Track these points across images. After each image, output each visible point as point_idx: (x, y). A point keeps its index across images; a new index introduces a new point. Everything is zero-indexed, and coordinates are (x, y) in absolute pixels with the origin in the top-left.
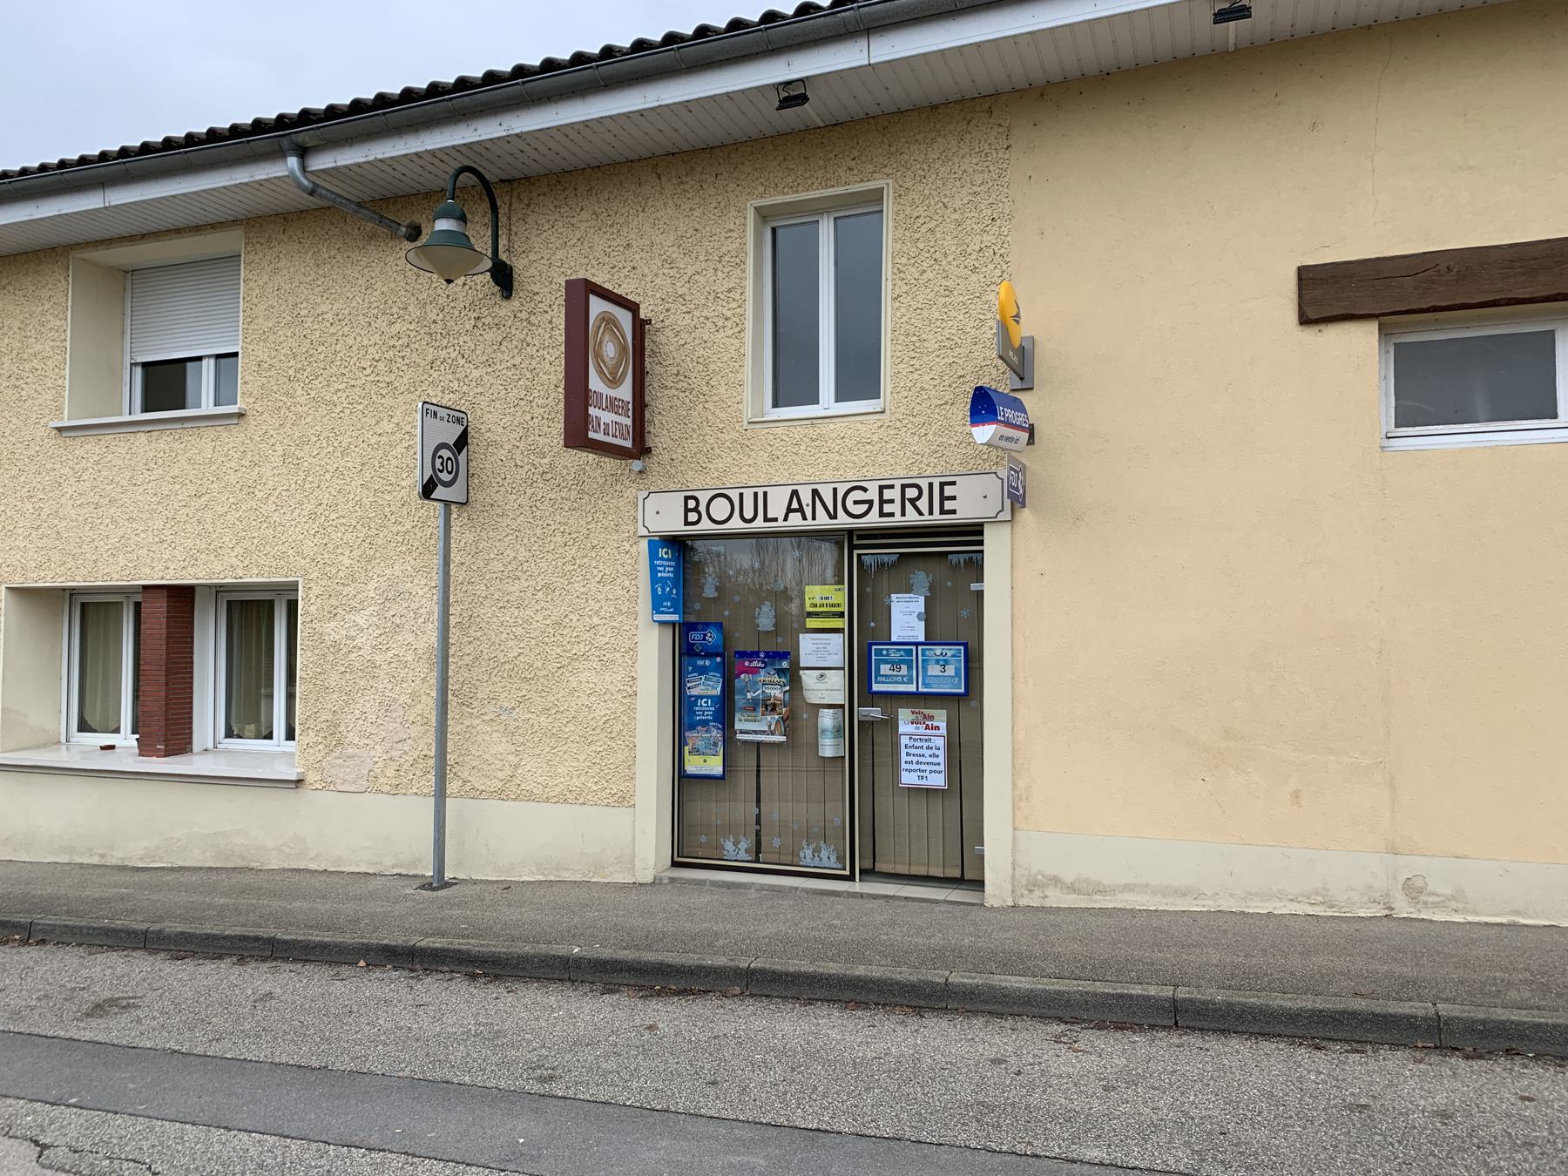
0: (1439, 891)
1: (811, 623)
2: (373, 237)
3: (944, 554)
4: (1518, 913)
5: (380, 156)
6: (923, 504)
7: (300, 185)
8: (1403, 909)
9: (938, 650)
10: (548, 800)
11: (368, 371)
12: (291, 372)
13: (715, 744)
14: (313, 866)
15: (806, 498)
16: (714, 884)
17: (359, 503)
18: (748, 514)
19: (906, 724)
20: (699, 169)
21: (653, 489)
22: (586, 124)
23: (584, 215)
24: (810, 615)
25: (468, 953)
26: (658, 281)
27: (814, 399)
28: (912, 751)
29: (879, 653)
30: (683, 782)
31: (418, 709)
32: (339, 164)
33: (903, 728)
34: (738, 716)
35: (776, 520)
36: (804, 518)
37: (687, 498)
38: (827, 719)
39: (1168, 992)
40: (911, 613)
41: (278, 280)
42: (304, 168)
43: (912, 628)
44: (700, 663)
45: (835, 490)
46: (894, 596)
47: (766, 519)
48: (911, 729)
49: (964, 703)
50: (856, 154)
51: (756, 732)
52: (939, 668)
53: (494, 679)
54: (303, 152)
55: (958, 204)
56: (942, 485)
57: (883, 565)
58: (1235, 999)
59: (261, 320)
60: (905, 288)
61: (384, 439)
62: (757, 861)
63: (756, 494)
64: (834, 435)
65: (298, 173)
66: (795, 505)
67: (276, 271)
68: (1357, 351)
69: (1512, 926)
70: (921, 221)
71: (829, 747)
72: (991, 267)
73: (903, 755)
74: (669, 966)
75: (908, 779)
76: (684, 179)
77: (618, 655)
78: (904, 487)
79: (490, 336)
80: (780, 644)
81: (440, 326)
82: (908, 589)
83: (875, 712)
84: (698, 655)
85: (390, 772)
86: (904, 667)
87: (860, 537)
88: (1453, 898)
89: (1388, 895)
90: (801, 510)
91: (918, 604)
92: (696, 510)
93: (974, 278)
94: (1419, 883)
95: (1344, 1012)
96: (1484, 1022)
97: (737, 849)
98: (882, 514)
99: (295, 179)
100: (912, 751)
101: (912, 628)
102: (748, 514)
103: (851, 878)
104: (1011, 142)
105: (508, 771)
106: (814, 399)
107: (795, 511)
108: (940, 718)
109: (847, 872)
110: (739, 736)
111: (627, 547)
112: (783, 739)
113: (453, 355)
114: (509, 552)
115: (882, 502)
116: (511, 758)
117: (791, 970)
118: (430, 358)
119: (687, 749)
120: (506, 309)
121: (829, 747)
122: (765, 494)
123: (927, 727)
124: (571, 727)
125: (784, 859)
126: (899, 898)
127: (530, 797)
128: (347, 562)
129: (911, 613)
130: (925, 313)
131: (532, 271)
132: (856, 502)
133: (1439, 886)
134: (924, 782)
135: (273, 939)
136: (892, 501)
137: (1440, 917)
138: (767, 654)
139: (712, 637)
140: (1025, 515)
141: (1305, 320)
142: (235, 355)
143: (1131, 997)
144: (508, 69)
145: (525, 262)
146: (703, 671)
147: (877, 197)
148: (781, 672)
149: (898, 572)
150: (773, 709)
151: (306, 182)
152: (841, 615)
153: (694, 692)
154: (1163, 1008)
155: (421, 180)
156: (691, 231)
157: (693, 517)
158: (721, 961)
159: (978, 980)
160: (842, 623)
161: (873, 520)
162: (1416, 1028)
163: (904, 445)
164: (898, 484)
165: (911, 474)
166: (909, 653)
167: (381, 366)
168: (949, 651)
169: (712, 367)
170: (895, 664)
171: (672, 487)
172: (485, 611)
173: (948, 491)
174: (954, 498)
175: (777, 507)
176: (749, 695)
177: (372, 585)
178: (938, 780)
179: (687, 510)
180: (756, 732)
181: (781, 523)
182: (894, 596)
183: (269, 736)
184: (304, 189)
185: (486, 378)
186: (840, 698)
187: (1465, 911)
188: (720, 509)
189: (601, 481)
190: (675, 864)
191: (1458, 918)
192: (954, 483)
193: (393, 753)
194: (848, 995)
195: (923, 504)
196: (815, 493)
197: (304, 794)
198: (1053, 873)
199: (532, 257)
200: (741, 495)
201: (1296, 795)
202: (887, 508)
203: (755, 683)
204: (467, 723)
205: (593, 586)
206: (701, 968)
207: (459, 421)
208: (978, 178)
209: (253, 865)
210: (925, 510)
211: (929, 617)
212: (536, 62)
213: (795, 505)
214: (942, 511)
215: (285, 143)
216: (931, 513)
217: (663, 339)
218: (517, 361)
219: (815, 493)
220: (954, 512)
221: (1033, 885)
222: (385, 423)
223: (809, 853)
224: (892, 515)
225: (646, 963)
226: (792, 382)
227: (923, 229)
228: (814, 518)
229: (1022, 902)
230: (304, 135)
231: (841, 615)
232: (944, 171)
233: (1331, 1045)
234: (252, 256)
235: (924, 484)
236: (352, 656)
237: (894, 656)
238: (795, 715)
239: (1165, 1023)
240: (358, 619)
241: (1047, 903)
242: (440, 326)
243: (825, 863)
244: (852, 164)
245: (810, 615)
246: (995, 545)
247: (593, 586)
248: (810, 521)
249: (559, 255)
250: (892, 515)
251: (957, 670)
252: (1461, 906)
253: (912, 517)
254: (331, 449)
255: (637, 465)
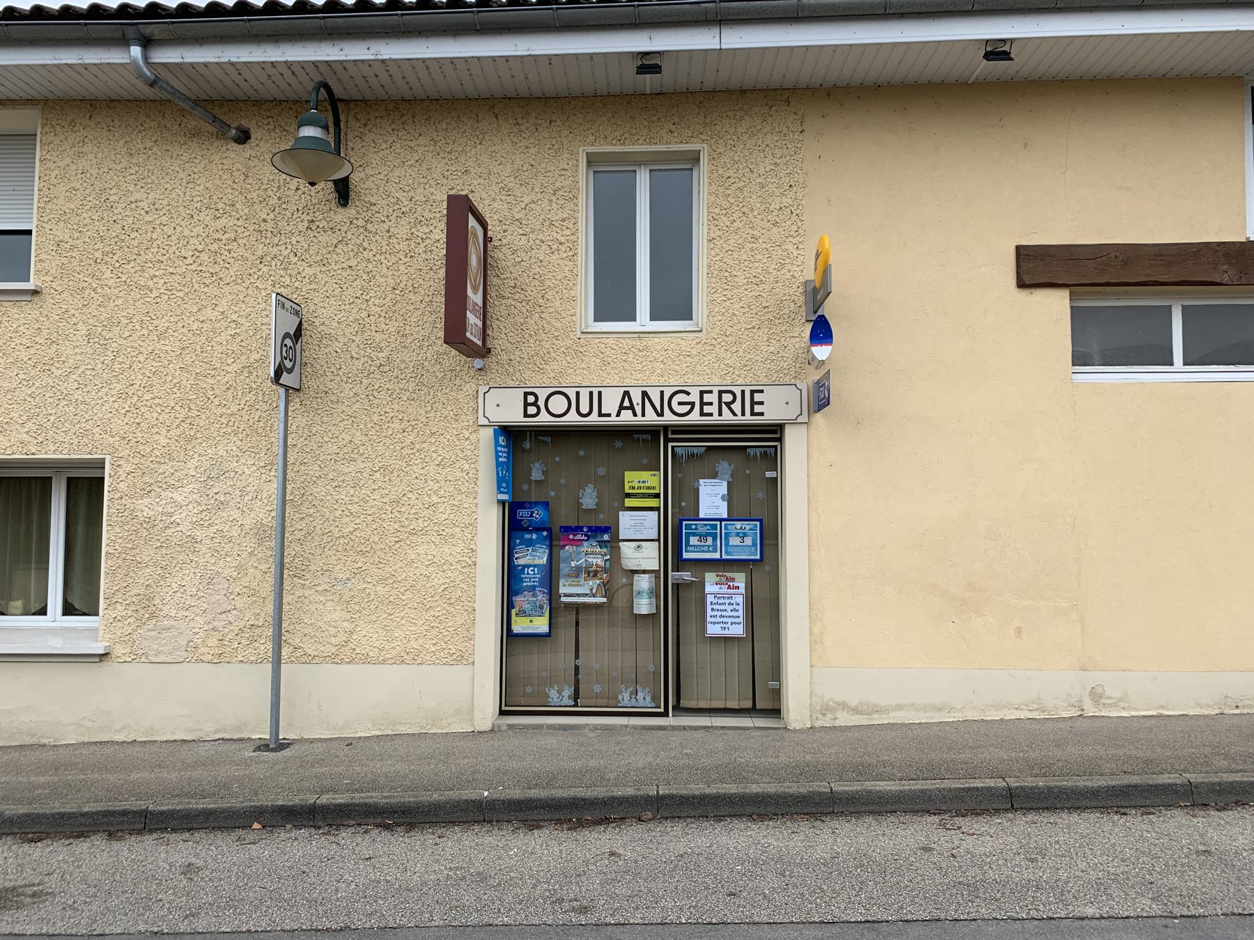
0: (1113, 695)
1: (629, 502)
2: (195, 134)
3: (752, 449)
4: (1162, 707)
5: (233, 60)
6: (737, 407)
7: (141, 75)
8: (1091, 710)
9: (738, 524)
10: (384, 662)
11: (190, 260)
12: (98, 255)
13: (541, 607)
14: (119, 737)
15: (637, 398)
16: (550, 727)
17: (179, 385)
18: (584, 410)
19: (712, 584)
20: (534, 115)
21: (492, 384)
22: (452, 60)
23: (422, 140)
24: (628, 495)
25: (375, 806)
26: (495, 205)
27: (633, 318)
28: (715, 607)
29: (688, 527)
30: (510, 640)
31: (245, 581)
32: (187, 60)
33: (710, 588)
34: (562, 582)
35: (609, 415)
36: (635, 415)
37: (526, 394)
38: (643, 583)
39: (1001, 783)
40: (716, 495)
41: (82, 164)
42: (145, 58)
43: (717, 507)
44: (527, 536)
45: (662, 392)
46: (701, 481)
47: (600, 415)
48: (716, 589)
49: (763, 570)
50: (676, 120)
51: (578, 595)
52: (739, 539)
53: (327, 553)
54: (147, 43)
55: (762, 171)
56: (752, 392)
57: (693, 455)
58: (1052, 784)
59: (61, 201)
60: (718, 233)
61: (206, 326)
62: (576, 705)
63: (591, 393)
64: (659, 348)
65: (141, 63)
66: (626, 403)
67: (80, 155)
68: (1054, 307)
69: (1160, 716)
70: (732, 180)
71: (644, 606)
72: (789, 223)
73: (709, 610)
74: (583, 799)
75: (713, 630)
76: (520, 121)
77: (457, 530)
78: (720, 393)
79: (324, 238)
80: (602, 520)
81: (269, 226)
82: (714, 475)
83: (686, 576)
84: (526, 530)
85: (213, 642)
86: (710, 539)
87: (674, 432)
88: (1120, 700)
89: (1081, 701)
90: (632, 408)
91: (722, 488)
92: (535, 404)
93: (775, 230)
94: (1099, 690)
95: (1129, 786)
96: (1219, 784)
97: (560, 696)
98: (702, 414)
99: (138, 68)
100: (715, 607)
101: (717, 507)
102: (584, 410)
103: (665, 714)
104: (804, 127)
105: (343, 637)
106: (633, 318)
107: (627, 408)
108: (740, 580)
109: (662, 710)
110: (563, 599)
111: (467, 434)
112: (604, 600)
113: (285, 253)
114: (344, 436)
115: (702, 404)
116: (346, 624)
117: (697, 793)
118: (260, 253)
119: (513, 612)
120: (341, 215)
121: (644, 606)
122: (600, 393)
123: (729, 587)
124: (409, 595)
125: (599, 702)
126: (716, 728)
127: (367, 660)
128: (164, 441)
129: (716, 495)
130: (736, 255)
131: (369, 184)
132: (680, 403)
133: (1113, 692)
134: (726, 632)
135: (146, 811)
136: (711, 404)
137: (1114, 714)
138: (590, 529)
139: (539, 514)
140: (818, 417)
141: (1022, 284)
142: (29, 232)
143: (977, 789)
144: (56, 6)
145: (362, 175)
146: (530, 543)
147: (695, 158)
148: (602, 544)
149: (704, 464)
150: (595, 575)
151: (148, 73)
152: (657, 496)
153: (521, 562)
154: (1002, 795)
155: (259, 87)
156: (526, 167)
157: (532, 410)
158: (630, 791)
159: (855, 787)
160: (652, 503)
161: (695, 418)
162: (1176, 792)
163: (719, 359)
164: (715, 390)
165: (725, 382)
166: (714, 527)
167: (204, 256)
168: (747, 526)
169: (548, 283)
170: (702, 537)
171: (511, 384)
172: (319, 490)
173: (757, 397)
174: (762, 403)
175: (611, 402)
176: (573, 564)
177: (192, 464)
178: (738, 630)
179: (526, 404)
180: (578, 595)
181: (613, 418)
182: (701, 481)
183: (43, 612)
184: (146, 79)
185: (320, 276)
186: (654, 564)
187: (1129, 708)
188: (558, 404)
189: (440, 375)
190: (502, 713)
191: (1125, 714)
192: (762, 391)
193: (216, 624)
194: (749, 810)
195: (737, 407)
196: (645, 394)
197: (106, 665)
198: (840, 700)
199: (369, 171)
200: (578, 393)
201: (1019, 631)
202: (707, 409)
203: (579, 553)
204: (299, 593)
205: (432, 468)
206: (614, 798)
207: (297, 313)
208: (778, 152)
209: (43, 741)
210: (738, 412)
211: (730, 498)
212: (56, 6)
213: (626, 403)
214: (753, 414)
215: (131, 32)
216: (743, 414)
217: (501, 256)
218: (353, 263)
219: (645, 394)
220: (762, 414)
221: (825, 710)
222: (209, 311)
223: (626, 696)
224: (711, 415)
225: (560, 799)
226: (613, 301)
227: (733, 187)
228: (643, 415)
229: (818, 724)
230: (153, 28)
231: (657, 496)
232: (750, 143)
233: (1128, 811)
234: (50, 137)
235: (572, 393)
236: (169, 532)
237: (701, 530)
238: (616, 578)
239: (1004, 806)
240: (175, 495)
241: (837, 723)
242: (269, 226)
243: (641, 703)
244: (673, 128)
245: (628, 495)
246: (794, 445)
247: (432, 468)
248: (639, 417)
249: (397, 172)
250: (711, 415)
251: (754, 544)
252: (1126, 705)
253: (727, 417)
254: (145, 332)
255: (478, 363)
